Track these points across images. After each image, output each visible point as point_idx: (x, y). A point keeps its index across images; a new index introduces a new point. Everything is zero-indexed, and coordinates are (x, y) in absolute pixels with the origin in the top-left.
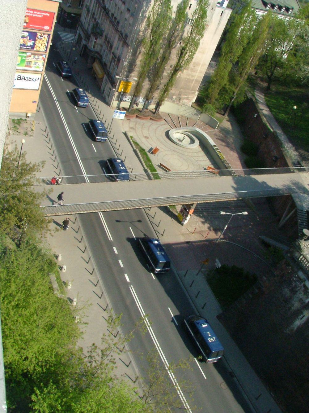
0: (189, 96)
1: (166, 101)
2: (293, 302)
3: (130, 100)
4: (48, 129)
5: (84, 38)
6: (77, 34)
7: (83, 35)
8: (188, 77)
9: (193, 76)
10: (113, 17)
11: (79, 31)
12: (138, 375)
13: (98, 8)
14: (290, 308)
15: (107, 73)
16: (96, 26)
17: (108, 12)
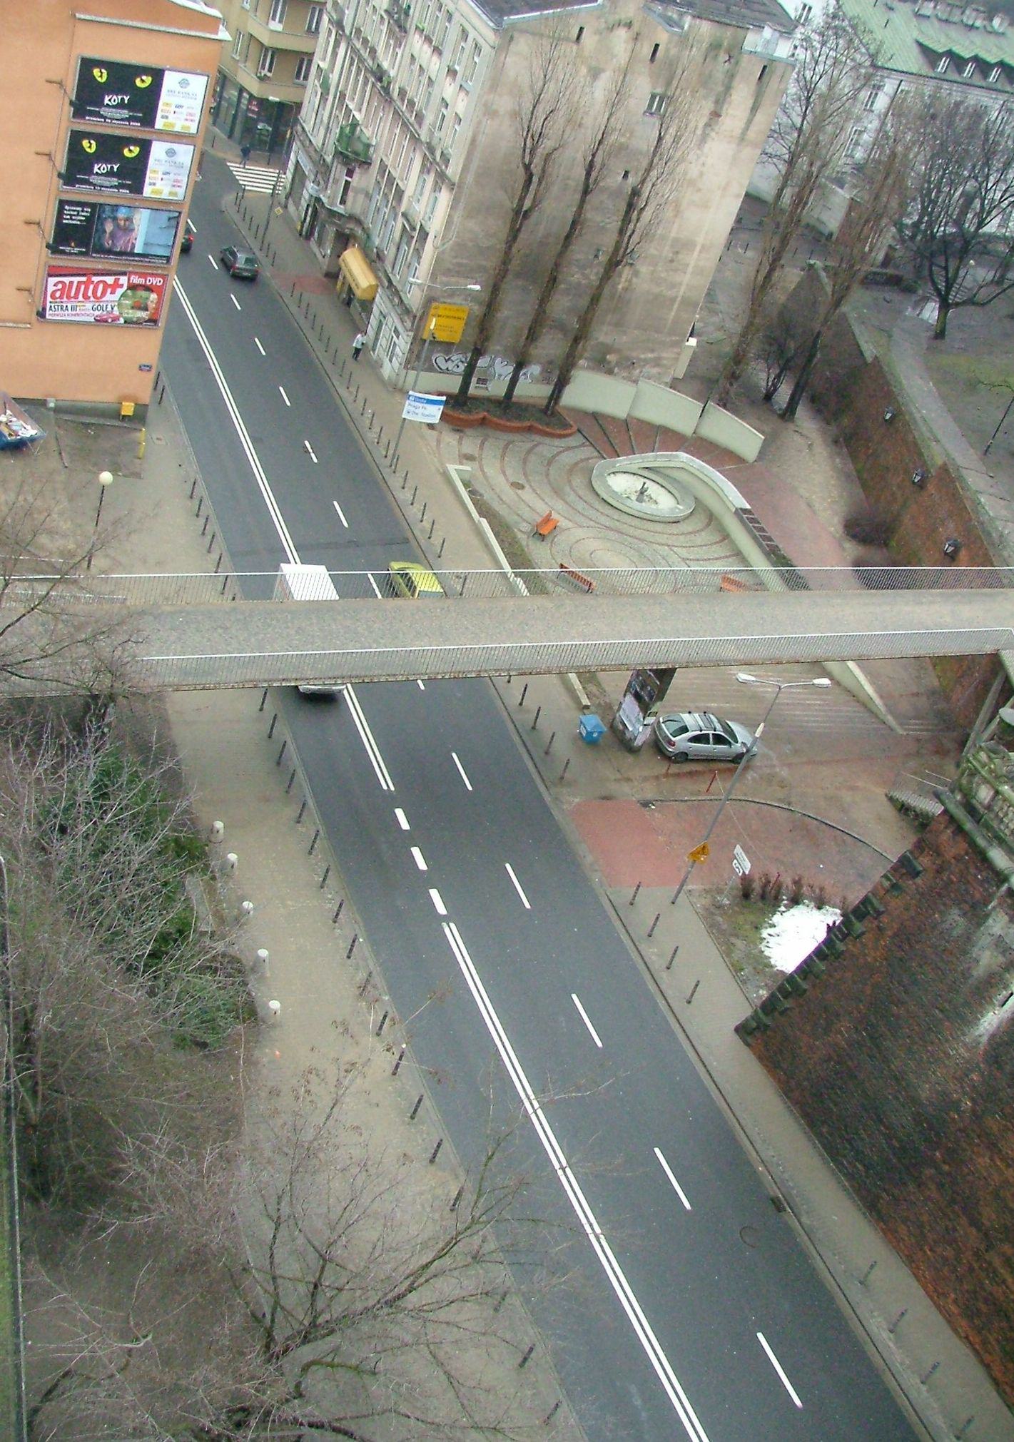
0: (664, 355)
1: (583, 368)
2: (975, 952)
3: (462, 367)
4: (201, 490)
5: (312, 177)
6: (291, 166)
7: (307, 167)
8: (656, 290)
9: (673, 286)
10: (403, 100)
11: (296, 154)
12: (423, 1091)
13: (358, 74)
14: (966, 974)
15: (386, 284)
16: (350, 134)
17: (389, 83)
